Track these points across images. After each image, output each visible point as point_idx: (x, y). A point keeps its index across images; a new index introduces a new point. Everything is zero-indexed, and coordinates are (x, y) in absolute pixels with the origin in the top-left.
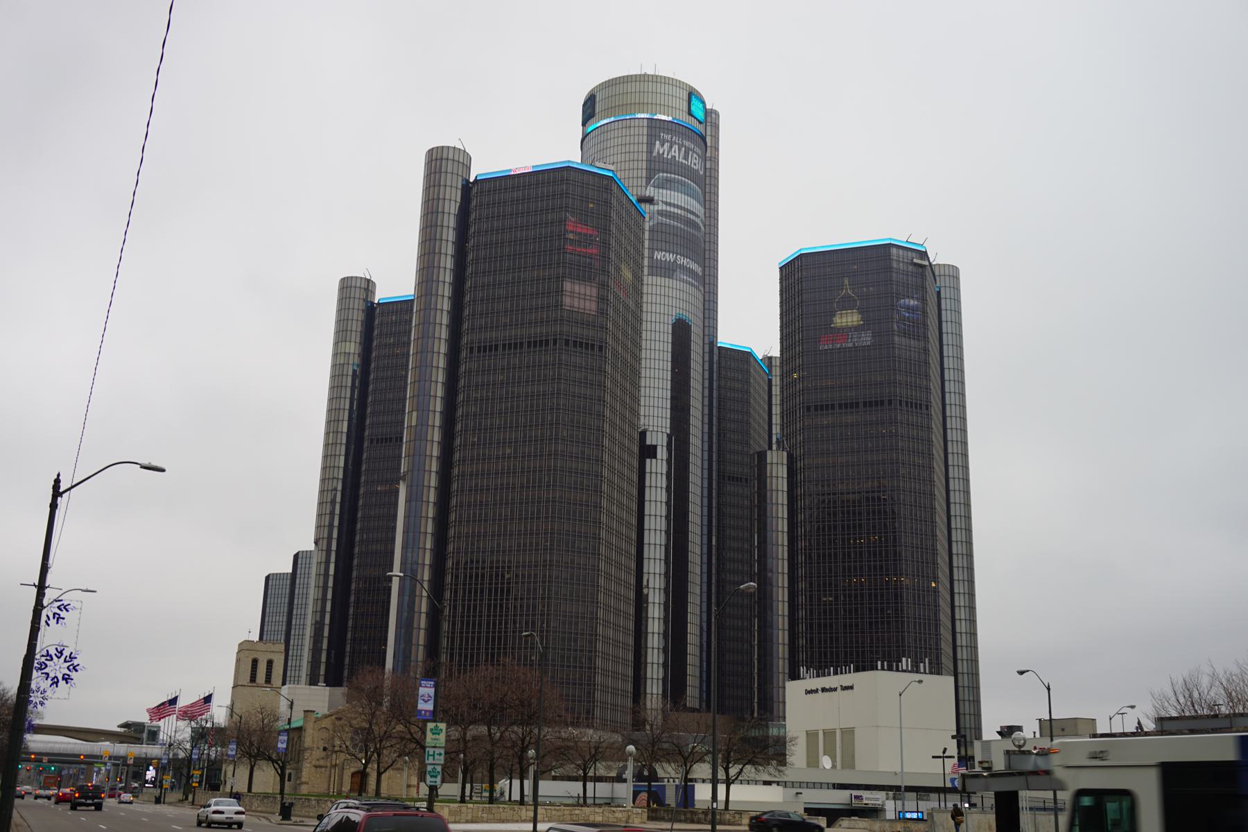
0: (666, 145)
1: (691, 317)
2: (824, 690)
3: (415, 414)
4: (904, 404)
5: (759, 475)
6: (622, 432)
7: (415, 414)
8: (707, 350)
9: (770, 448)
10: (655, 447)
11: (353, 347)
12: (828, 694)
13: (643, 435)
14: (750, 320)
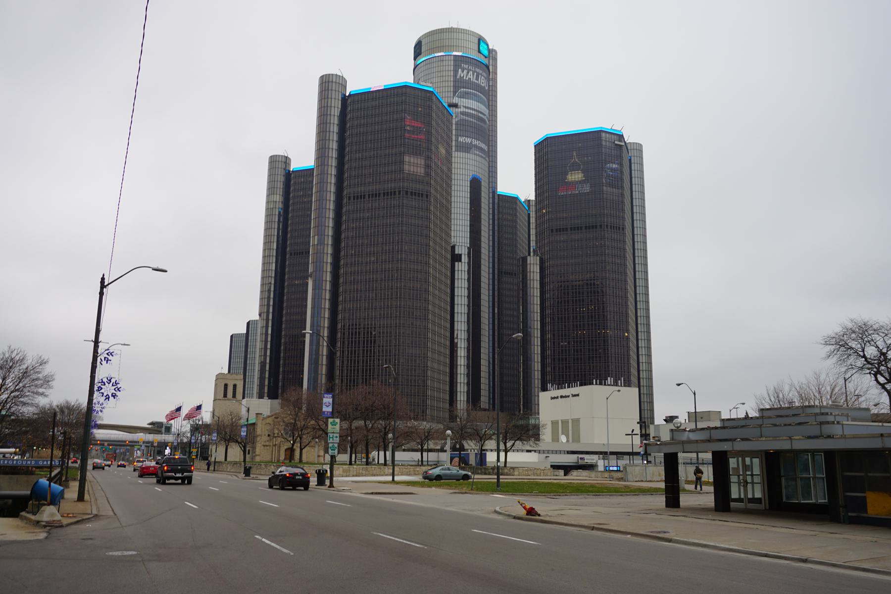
0: (465, 72)
1: (481, 176)
2: (562, 397)
10: (461, 255)
11: (278, 198)
12: (563, 399)
13: (453, 248)
14: (517, 179)
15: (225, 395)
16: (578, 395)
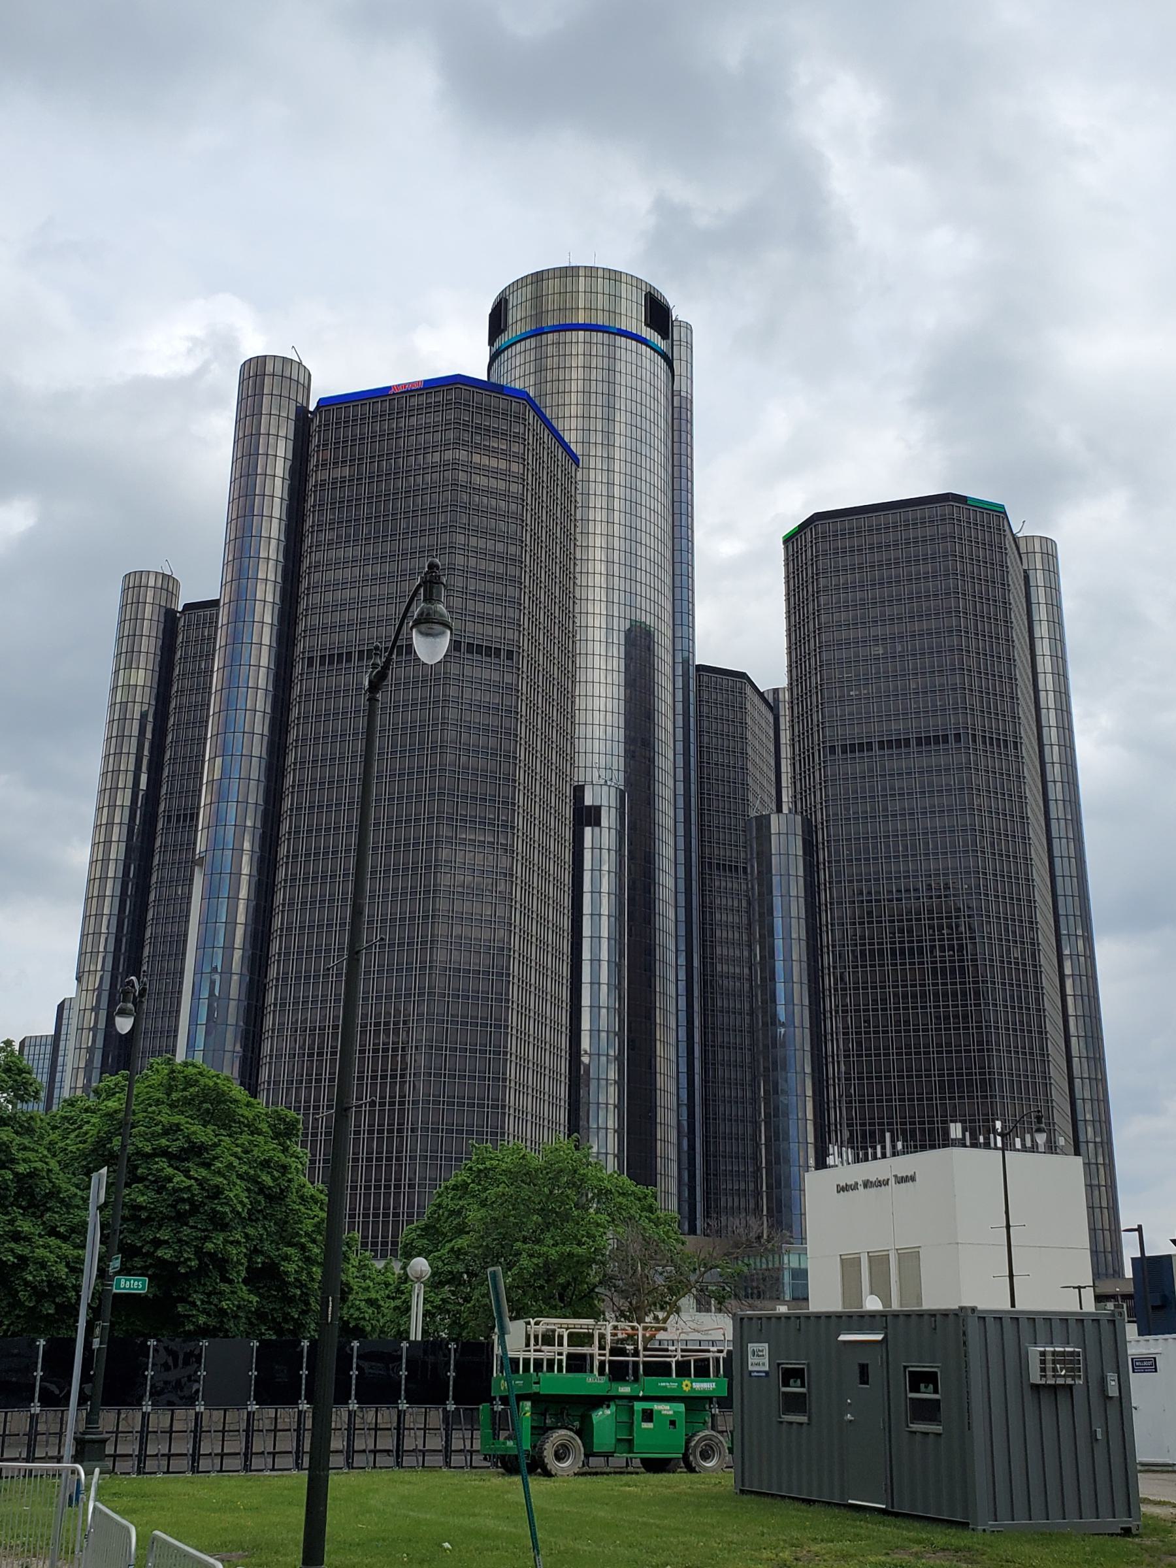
2: (867, 1184)
3: (219, 760)
4: (979, 740)
5: (760, 854)
6: (546, 784)
7: (219, 760)
8: (679, 671)
9: (779, 810)
10: (597, 809)
11: (142, 677)
12: (873, 1191)
13: (579, 791)
14: (743, 624)
15: (528, 1345)
16: (913, 1179)
